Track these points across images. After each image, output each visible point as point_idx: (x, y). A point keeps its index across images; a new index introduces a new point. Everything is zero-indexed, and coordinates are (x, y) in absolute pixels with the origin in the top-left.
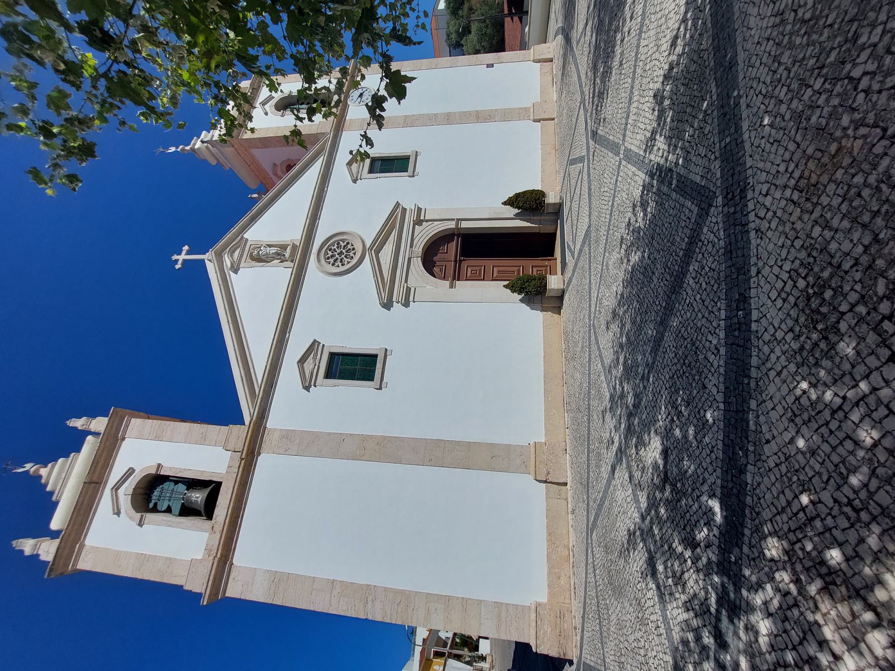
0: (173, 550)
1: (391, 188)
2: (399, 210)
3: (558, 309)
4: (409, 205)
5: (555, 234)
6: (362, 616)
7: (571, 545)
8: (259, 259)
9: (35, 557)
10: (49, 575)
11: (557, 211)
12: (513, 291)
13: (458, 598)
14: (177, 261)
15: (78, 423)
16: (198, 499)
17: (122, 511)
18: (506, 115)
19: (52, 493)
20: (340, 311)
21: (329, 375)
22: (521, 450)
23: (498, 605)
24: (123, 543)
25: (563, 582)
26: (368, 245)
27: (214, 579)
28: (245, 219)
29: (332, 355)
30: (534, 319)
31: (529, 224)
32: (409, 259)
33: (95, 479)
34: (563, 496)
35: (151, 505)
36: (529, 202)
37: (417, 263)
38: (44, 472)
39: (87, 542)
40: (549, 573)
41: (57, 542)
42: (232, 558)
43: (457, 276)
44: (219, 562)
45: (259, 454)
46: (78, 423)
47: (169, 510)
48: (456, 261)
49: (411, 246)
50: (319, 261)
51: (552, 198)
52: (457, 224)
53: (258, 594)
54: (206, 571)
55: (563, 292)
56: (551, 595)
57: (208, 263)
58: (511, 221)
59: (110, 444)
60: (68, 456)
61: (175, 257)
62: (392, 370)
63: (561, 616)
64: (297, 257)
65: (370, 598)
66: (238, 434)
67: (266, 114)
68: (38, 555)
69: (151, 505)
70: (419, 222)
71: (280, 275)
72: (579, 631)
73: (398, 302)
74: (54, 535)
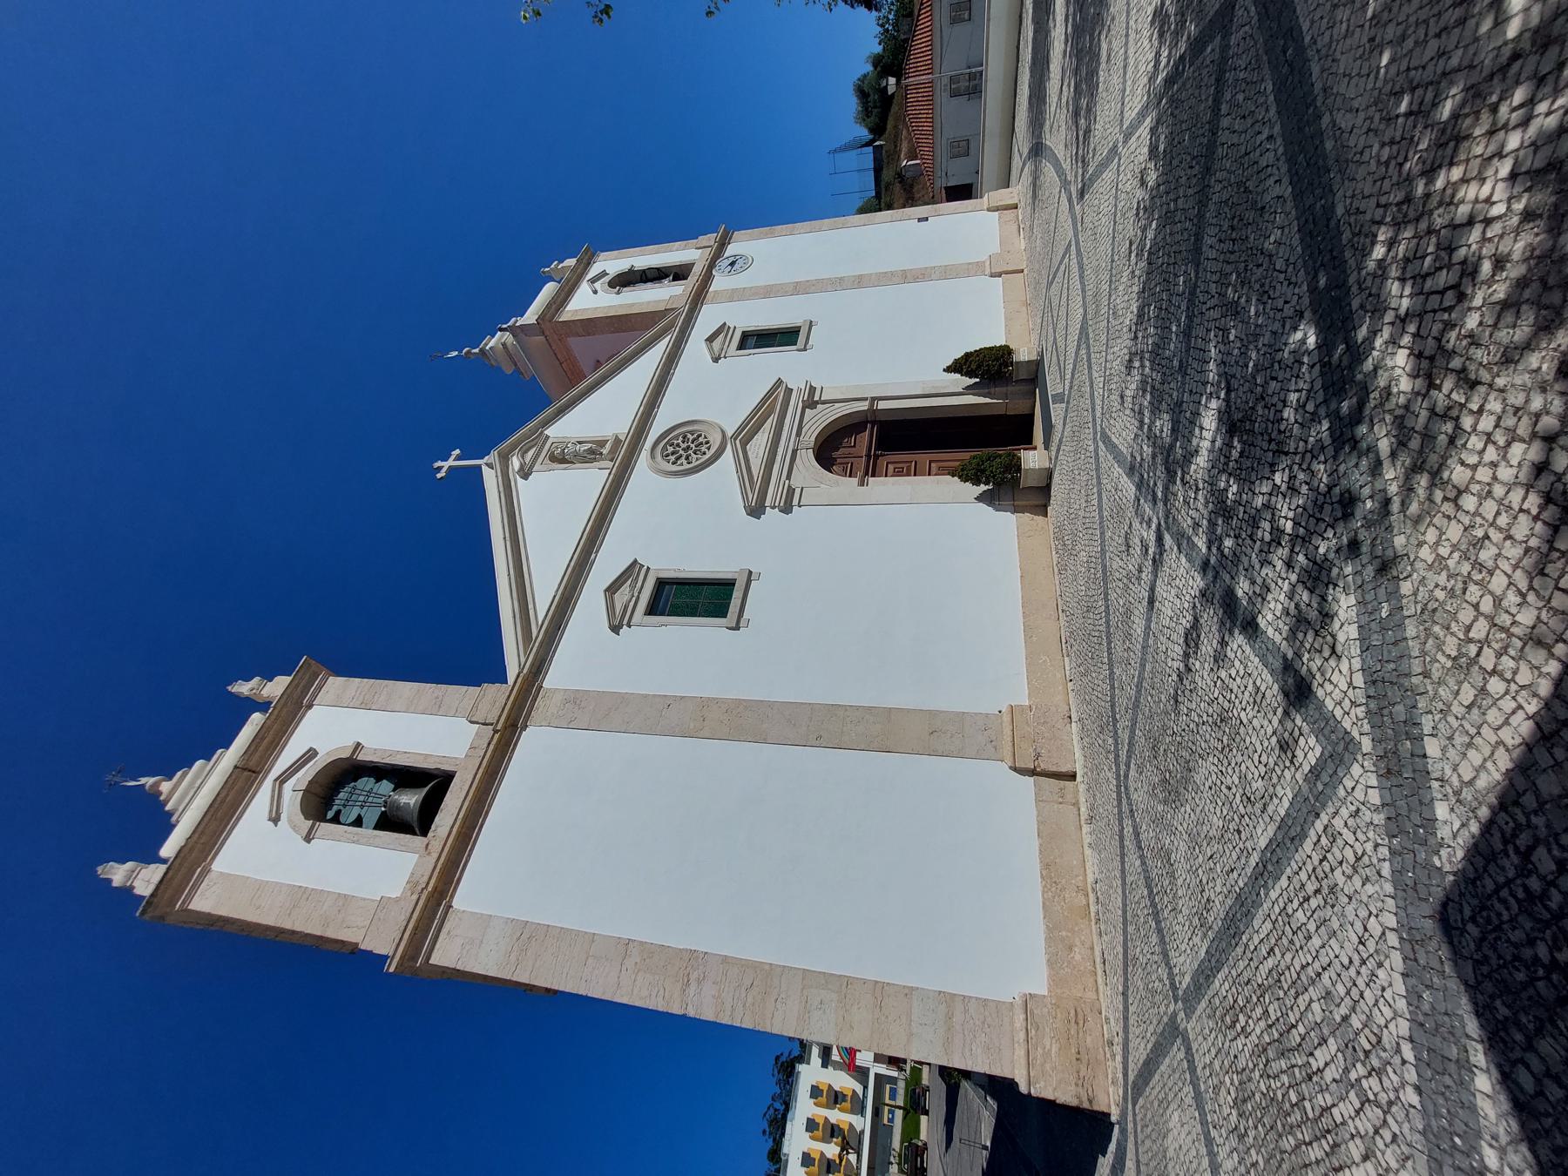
0: (350, 883)
3: (1042, 509)
4: (796, 383)
5: (1033, 415)
6: (676, 1009)
7: (1090, 879)
8: (561, 458)
9: (127, 891)
10: (143, 913)
11: (1034, 375)
12: (965, 479)
13: (865, 982)
14: (440, 469)
15: (243, 688)
16: (405, 798)
17: (284, 817)
18: (935, 734)
19: (170, 814)
20: (680, 521)
21: (652, 610)
22: (985, 723)
23: (948, 999)
25: (1078, 957)
26: (730, 433)
27: (415, 928)
28: (550, 411)
29: (661, 584)
30: (1005, 524)
31: (988, 400)
32: (795, 452)
33: (251, 764)
34: (1069, 797)
35: (330, 814)
36: (988, 366)
37: (807, 459)
38: (165, 787)
39: (214, 867)
40: (1049, 940)
41: (163, 868)
42: (452, 897)
43: (872, 470)
44: (428, 900)
45: (525, 727)
46: (243, 688)
47: (358, 822)
48: (869, 456)
49: (799, 434)
50: (653, 456)
51: (1024, 354)
52: (872, 404)
53: (487, 961)
54: (403, 918)
55: (1049, 474)
56: (1056, 981)
57: (484, 468)
58: (957, 393)
60: (209, 759)
62: (758, 604)
63: (1078, 1019)
64: (620, 457)
65: (693, 976)
66: (493, 698)
67: (595, 292)
68: (132, 888)
69: (330, 814)
70: (811, 403)
71: (592, 480)
72: (1118, 1049)
73: (773, 507)
74: (164, 861)
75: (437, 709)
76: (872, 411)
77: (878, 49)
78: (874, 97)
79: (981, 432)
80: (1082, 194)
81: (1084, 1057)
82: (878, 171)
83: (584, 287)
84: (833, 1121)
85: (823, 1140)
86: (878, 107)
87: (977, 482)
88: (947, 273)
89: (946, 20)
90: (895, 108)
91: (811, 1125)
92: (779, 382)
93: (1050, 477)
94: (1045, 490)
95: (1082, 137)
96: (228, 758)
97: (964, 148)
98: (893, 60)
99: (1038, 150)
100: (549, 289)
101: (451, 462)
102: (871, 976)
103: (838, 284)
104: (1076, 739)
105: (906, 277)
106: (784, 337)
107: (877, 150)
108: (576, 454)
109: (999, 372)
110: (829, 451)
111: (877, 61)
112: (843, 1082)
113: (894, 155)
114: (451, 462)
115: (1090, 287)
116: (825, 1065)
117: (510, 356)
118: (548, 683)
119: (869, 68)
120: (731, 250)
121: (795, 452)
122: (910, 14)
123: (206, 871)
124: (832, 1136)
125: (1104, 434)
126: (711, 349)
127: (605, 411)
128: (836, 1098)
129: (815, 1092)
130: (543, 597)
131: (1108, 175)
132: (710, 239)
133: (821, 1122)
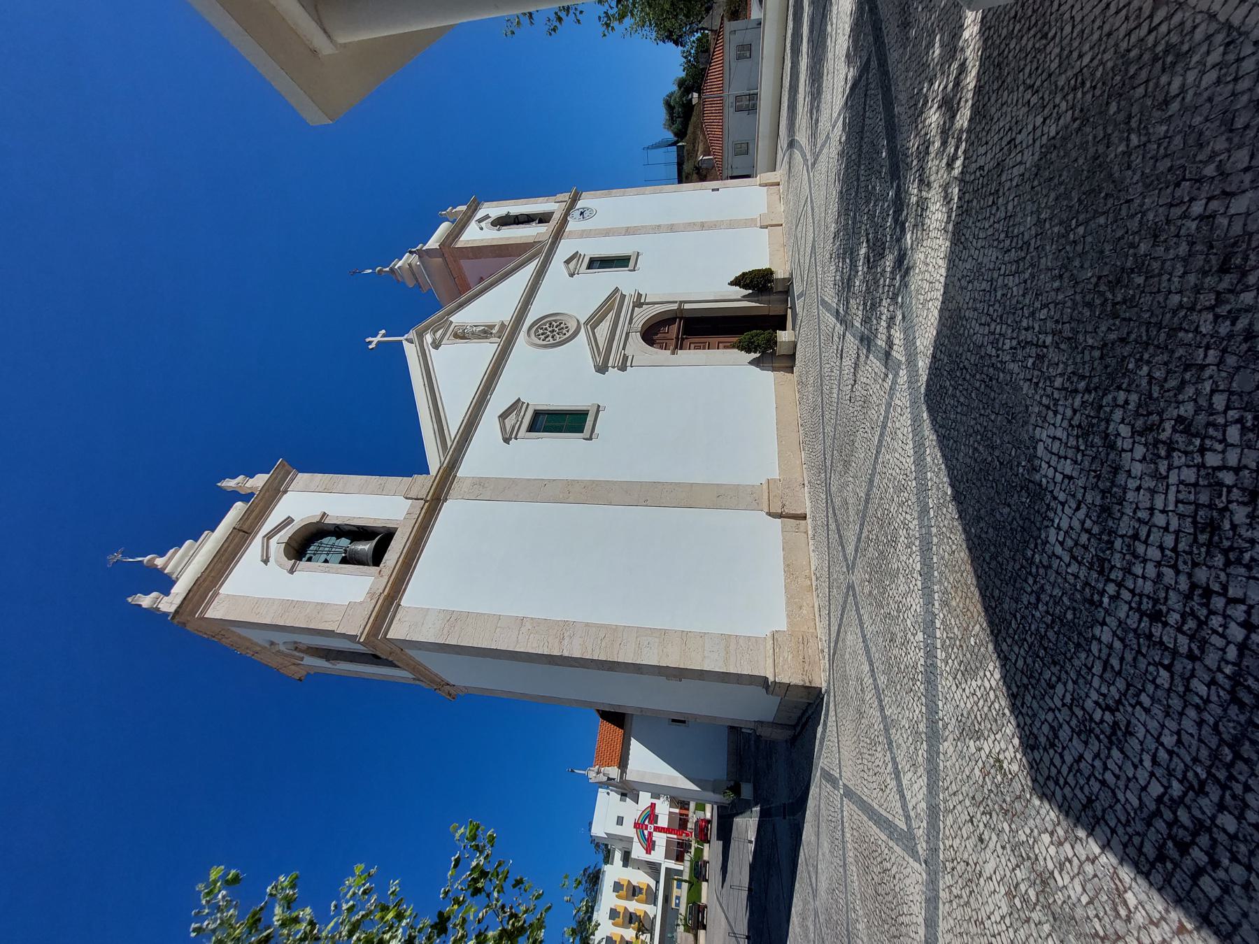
1: (609, 279)
2: (618, 295)
3: (790, 369)
7: (813, 568)
8: (461, 335)
11: (786, 289)
14: (370, 343)
15: (229, 484)
18: (720, 497)
23: (726, 638)
24: (265, 590)
26: (582, 321)
27: (377, 617)
30: (767, 379)
32: (627, 334)
33: (245, 528)
34: (802, 529)
36: (757, 282)
37: (636, 340)
43: (679, 345)
44: (385, 600)
45: (446, 500)
46: (229, 484)
48: (677, 338)
49: (630, 323)
54: (366, 613)
56: (790, 624)
58: (736, 299)
59: (273, 493)
61: (370, 339)
63: (804, 641)
64: (507, 337)
66: (422, 485)
70: (638, 304)
75: (381, 491)
76: (680, 310)
77: (683, 74)
78: (678, 109)
79: (752, 322)
80: (814, 164)
81: (807, 660)
82: (680, 165)
83: (473, 225)
84: (631, 910)
85: (623, 926)
86: (683, 114)
87: (749, 351)
88: (732, 225)
89: (733, 54)
90: (694, 119)
91: (614, 914)
92: (617, 290)
93: (795, 347)
94: (792, 357)
95: (814, 135)
96: (212, 541)
97: (745, 149)
98: (695, 80)
99: (792, 144)
100: (444, 227)
101: (379, 338)
102: (679, 627)
103: (658, 229)
104: (807, 495)
105: (703, 226)
106: (621, 262)
107: (680, 149)
108: (473, 333)
109: (765, 286)
110: (652, 333)
111: (681, 83)
112: (640, 878)
113: (694, 152)
114: (379, 338)
115: (817, 219)
116: (626, 864)
117: (414, 274)
118: (461, 473)
119: (675, 88)
120: (580, 204)
121: (627, 334)
122: (707, 51)
123: (216, 594)
124: (630, 922)
125: (823, 300)
126: (568, 269)
127: (495, 304)
128: (634, 892)
129: (617, 887)
130: (454, 424)
131: (825, 151)
132: (566, 196)
133: (625, 884)
